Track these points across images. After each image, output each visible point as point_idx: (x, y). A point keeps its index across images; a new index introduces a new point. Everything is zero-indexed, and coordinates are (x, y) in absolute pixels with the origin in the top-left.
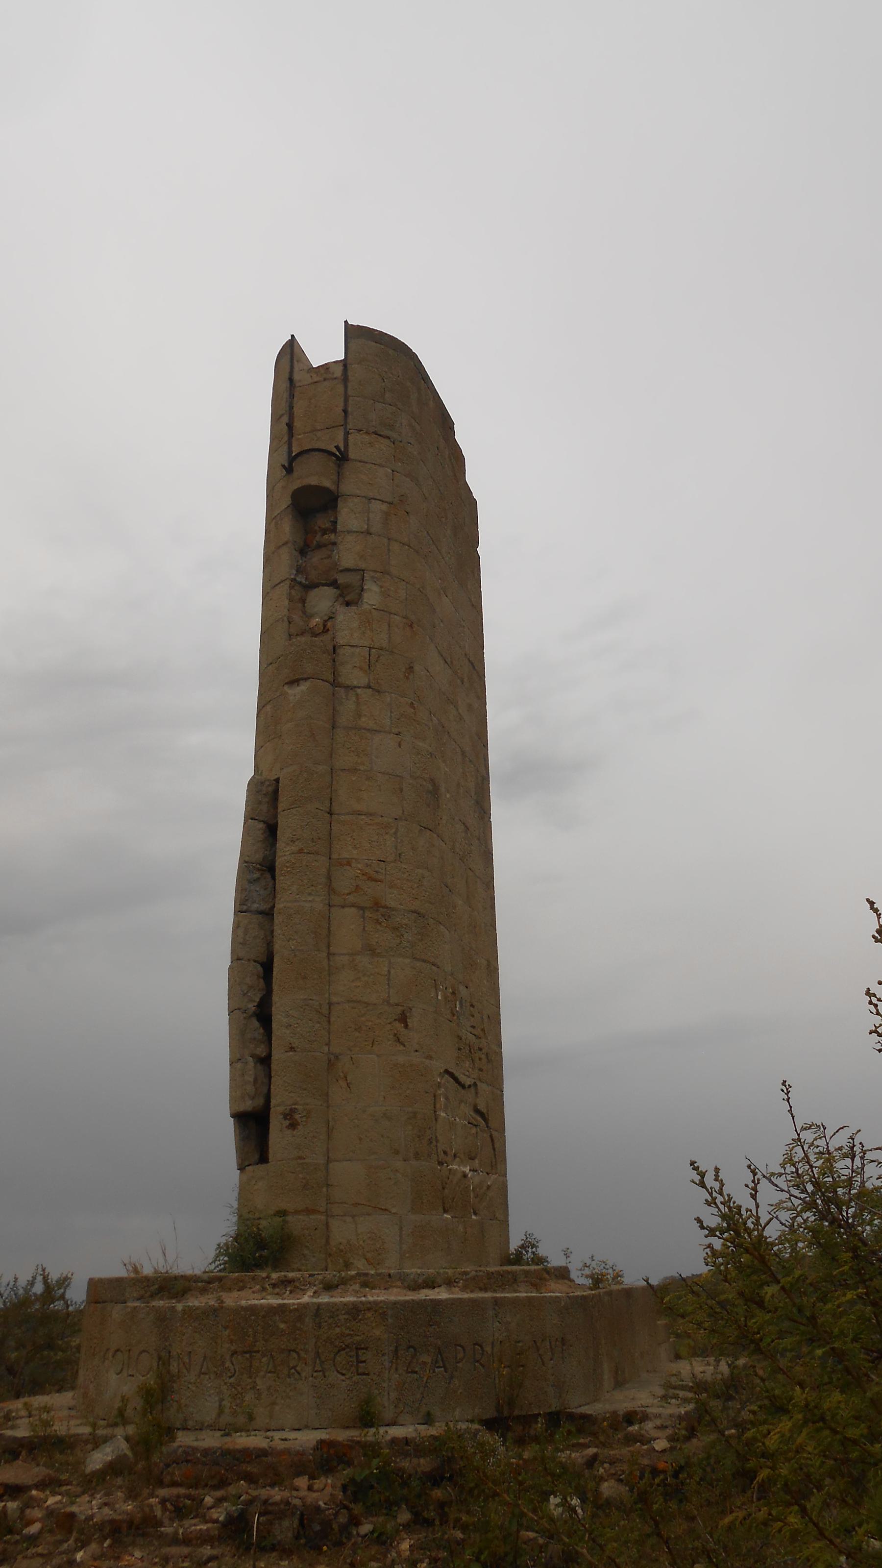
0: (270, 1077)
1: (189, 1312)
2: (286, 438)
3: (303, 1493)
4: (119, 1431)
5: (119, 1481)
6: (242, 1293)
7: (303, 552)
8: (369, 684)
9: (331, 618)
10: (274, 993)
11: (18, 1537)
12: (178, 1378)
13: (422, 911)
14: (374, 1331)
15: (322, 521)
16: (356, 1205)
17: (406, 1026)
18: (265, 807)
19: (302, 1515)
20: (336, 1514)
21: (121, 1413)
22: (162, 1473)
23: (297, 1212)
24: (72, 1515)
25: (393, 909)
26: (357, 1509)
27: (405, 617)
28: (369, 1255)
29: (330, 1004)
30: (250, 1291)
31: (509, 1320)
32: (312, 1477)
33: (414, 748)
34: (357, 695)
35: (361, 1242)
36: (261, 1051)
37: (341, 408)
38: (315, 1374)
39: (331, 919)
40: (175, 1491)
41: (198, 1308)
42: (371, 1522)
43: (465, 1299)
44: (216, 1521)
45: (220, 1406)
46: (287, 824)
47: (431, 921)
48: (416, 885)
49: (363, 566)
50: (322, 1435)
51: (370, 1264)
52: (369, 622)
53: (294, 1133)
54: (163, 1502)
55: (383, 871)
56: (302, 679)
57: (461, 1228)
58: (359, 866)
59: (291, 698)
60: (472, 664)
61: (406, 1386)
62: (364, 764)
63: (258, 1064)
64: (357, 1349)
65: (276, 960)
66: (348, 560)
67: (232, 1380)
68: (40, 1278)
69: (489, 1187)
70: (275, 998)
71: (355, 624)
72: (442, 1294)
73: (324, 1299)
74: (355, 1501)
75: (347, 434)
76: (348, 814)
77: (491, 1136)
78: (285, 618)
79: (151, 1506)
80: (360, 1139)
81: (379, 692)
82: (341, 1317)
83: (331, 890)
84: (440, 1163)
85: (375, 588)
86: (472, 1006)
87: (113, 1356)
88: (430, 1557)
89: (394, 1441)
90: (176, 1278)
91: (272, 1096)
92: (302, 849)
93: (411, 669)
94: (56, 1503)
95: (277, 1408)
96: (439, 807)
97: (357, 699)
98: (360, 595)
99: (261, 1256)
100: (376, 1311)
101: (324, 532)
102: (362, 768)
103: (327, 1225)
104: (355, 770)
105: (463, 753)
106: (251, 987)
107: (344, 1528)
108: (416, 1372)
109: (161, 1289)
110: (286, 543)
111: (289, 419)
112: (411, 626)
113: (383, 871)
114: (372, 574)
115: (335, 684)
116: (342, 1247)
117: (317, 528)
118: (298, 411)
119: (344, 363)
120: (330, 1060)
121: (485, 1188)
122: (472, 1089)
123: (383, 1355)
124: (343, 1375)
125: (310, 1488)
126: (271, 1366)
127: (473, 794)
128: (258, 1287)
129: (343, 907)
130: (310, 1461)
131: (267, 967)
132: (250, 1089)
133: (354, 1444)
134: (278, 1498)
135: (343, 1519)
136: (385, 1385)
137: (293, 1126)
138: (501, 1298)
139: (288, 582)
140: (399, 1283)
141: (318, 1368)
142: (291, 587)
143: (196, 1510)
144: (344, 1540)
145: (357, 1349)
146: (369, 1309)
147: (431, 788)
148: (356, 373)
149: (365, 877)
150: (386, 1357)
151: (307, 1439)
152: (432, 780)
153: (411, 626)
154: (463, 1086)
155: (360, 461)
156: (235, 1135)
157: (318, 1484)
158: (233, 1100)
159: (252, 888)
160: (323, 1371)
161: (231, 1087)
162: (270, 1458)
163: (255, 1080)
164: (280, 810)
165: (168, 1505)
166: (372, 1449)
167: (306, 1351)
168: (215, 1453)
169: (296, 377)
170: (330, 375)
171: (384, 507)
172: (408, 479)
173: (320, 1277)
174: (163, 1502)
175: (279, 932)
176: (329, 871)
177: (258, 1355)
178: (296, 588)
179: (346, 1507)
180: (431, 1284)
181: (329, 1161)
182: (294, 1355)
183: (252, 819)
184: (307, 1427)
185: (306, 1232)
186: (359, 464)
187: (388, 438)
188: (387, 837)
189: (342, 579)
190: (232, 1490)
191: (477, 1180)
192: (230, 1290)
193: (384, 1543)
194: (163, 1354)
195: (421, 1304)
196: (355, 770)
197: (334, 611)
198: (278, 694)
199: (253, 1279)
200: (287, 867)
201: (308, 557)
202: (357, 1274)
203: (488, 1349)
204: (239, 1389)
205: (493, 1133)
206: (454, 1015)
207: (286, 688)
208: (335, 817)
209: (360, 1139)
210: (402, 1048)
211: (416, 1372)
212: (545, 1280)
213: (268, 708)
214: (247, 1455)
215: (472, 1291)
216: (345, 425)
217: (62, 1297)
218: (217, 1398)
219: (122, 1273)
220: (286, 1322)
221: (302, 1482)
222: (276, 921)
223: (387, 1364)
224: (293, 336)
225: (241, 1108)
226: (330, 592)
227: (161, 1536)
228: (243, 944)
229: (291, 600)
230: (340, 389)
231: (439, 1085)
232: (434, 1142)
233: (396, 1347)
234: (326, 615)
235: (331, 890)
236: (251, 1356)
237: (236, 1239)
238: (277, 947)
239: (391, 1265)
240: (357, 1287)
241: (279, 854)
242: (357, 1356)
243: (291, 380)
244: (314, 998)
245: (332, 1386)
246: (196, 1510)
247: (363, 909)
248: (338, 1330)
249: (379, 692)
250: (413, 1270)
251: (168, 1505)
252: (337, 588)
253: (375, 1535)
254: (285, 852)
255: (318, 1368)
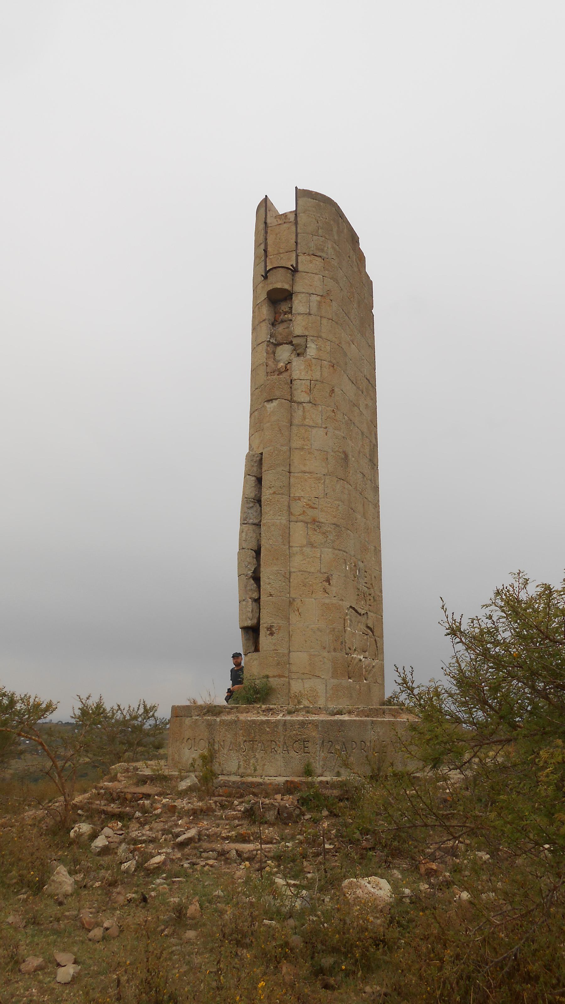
0: (260, 609)
1: (223, 722)
2: (263, 258)
3: (279, 800)
4: (192, 774)
5: (194, 794)
6: (249, 714)
7: (273, 325)
8: (310, 400)
9: (289, 363)
10: (262, 566)
11: (151, 815)
12: (219, 752)
13: (339, 524)
14: (312, 733)
15: (284, 307)
16: (303, 674)
17: (330, 584)
18: (255, 469)
19: (279, 809)
20: (294, 810)
21: (192, 765)
22: (214, 791)
23: (274, 677)
24: (175, 806)
25: (322, 523)
26: (304, 809)
27: (330, 362)
28: (310, 699)
29: (290, 573)
30: (252, 713)
31: (379, 731)
32: (283, 795)
33: (334, 435)
34: (303, 407)
35: (306, 692)
36: (255, 596)
37: (294, 240)
38: (284, 752)
39: (290, 528)
40: (221, 798)
41: (227, 720)
42: (310, 815)
43: (357, 720)
44: (240, 811)
45: (239, 765)
46: (267, 479)
47: (343, 529)
48: (335, 510)
49: (307, 334)
50: (288, 779)
51: (311, 703)
52: (310, 366)
53: (272, 637)
54: (215, 802)
55: (317, 503)
56: (274, 399)
57: (358, 687)
58: (305, 500)
59: (268, 410)
60: (368, 380)
61: (328, 759)
62: (307, 445)
63: (254, 603)
64: (304, 741)
65: (262, 549)
66: (298, 330)
67: (244, 753)
68: (142, 706)
69: (373, 667)
70: (262, 569)
71: (302, 367)
72: (346, 717)
73: (288, 718)
74: (303, 805)
75: (297, 256)
76: (299, 473)
77: (375, 640)
78: (265, 364)
79: (210, 803)
80: (306, 641)
81: (315, 405)
82: (296, 726)
83: (290, 513)
84: (347, 654)
85: (313, 346)
86: (366, 572)
87: (186, 741)
88: (336, 829)
89: (321, 782)
90: (215, 706)
91: (261, 619)
92: (275, 492)
93: (333, 391)
94: (167, 802)
95: (266, 766)
96: (348, 466)
97: (304, 409)
98: (305, 350)
99: (256, 698)
100: (313, 724)
101: (285, 313)
102: (306, 447)
103: (289, 682)
104: (302, 449)
105: (362, 433)
106: (249, 563)
107: (298, 816)
108: (332, 753)
109: (208, 711)
110: (264, 320)
111: (265, 246)
112: (333, 366)
113: (317, 503)
114: (312, 338)
115: (291, 401)
116: (296, 694)
117: (281, 311)
118: (270, 242)
119: (296, 213)
120: (290, 601)
121: (371, 667)
122: (365, 616)
123: (317, 744)
124: (297, 753)
125: (282, 800)
126: (263, 747)
127: (368, 456)
128: (256, 711)
129: (296, 522)
130: (282, 788)
131: (258, 552)
132: (250, 615)
133: (302, 783)
134: (268, 802)
135: (297, 812)
136: (317, 758)
137: (272, 634)
138: (375, 720)
139: (266, 343)
140: (324, 712)
141: (285, 749)
142: (268, 346)
143: (231, 806)
144: (298, 821)
145: (304, 741)
146: (310, 723)
147: (343, 456)
148: (302, 219)
149: (308, 506)
150: (318, 746)
151: (281, 780)
152: (344, 452)
153: (333, 366)
154: (360, 614)
155: (305, 272)
156: (242, 637)
157: (286, 797)
158: (241, 620)
159: (250, 511)
160: (288, 750)
161: (240, 614)
162: (263, 786)
163: (252, 611)
164: (263, 470)
165: (218, 803)
166: (311, 785)
167: (280, 742)
168: (238, 783)
169: (268, 221)
170: (288, 220)
171: (318, 298)
172: (332, 281)
173: (286, 708)
174: (215, 802)
175: (264, 535)
176: (289, 503)
177: (257, 743)
178: (270, 346)
179: (298, 808)
180: (340, 713)
181: (289, 652)
182: (274, 743)
183: (249, 475)
184: (280, 775)
185: (279, 686)
186: (304, 274)
187: (320, 257)
188: (320, 485)
189: (295, 341)
190: (247, 798)
191: (367, 663)
192: (242, 713)
193: (316, 823)
194: (211, 741)
195: (336, 722)
196: (302, 449)
197: (291, 359)
198: (261, 406)
199: (253, 708)
200: (268, 501)
201: (277, 327)
202: (304, 707)
203: (368, 744)
204: (248, 757)
205: (376, 638)
206: (355, 577)
207: (266, 403)
208: (292, 474)
209: (306, 641)
210: (327, 595)
211: (332, 753)
212: (401, 714)
213: (256, 413)
214: (253, 784)
215: (361, 717)
216: (296, 250)
217: (153, 716)
218: (237, 761)
219: (188, 703)
220: (269, 728)
221: (278, 797)
222: (262, 529)
223: (318, 749)
224: (266, 196)
225: (246, 624)
226: (288, 347)
227: (215, 816)
228: (245, 541)
229: (267, 353)
230: (294, 228)
231: (347, 614)
232: (344, 643)
233: (323, 741)
234: (287, 361)
235: (290, 513)
236: (253, 743)
237: (124, 722)
238: (262, 543)
239: (321, 703)
240: (304, 713)
241: (263, 494)
242: (304, 744)
243: (266, 223)
244: (282, 569)
245: (292, 757)
246: (231, 806)
247: (307, 523)
248: (294, 732)
249: (315, 405)
250: (332, 706)
251: (218, 803)
252: (293, 345)
253: (312, 819)
254: (266, 494)
255: (285, 749)
